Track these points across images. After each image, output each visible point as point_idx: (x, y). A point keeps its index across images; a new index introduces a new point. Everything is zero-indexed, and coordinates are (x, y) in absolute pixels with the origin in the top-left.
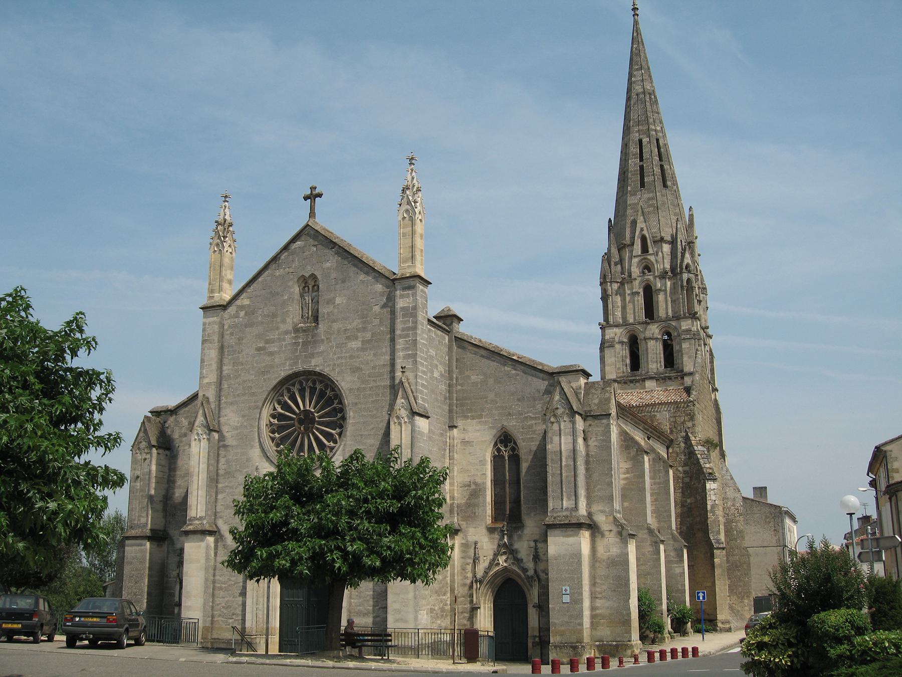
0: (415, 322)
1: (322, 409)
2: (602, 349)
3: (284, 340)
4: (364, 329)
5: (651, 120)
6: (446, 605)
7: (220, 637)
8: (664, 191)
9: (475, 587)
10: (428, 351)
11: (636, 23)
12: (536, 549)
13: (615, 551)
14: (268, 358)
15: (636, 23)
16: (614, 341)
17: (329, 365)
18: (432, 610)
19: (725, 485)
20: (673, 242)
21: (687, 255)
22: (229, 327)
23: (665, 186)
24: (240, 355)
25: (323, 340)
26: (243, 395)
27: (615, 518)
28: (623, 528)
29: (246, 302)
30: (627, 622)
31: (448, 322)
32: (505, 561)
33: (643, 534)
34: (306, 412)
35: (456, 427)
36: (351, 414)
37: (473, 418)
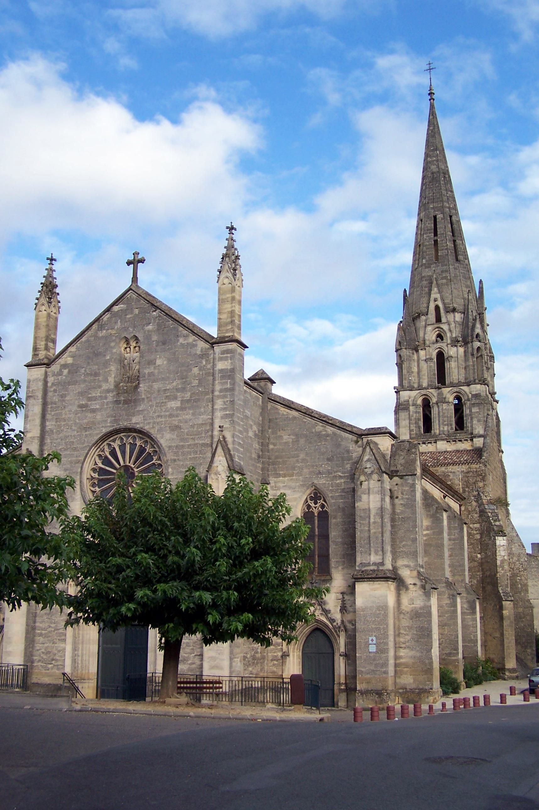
0: (233, 384)
1: (142, 464)
2: (396, 412)
3: (106, 398)
4: (183, 390)
5: (445, 198)
6: (257, 653)
7: (39, 682)
8: (457, 265)
10: (244, 412)
13: (419, 603)
14: (89, 415)
15: (432, 107)
16: (409, 404)
17: (149, 423)
18: (245, 658)
19: (511, 542)
20: (465, 312)
21: (478, 325)
22: (53, 384)
23: (457, 260)
24: (63, 412)
25: (143, 399)
29: (70, 360)
30: (429, 671)
33: (442, 587)
34: (127, 468)
36: (170, 470)
37: (285, 476)
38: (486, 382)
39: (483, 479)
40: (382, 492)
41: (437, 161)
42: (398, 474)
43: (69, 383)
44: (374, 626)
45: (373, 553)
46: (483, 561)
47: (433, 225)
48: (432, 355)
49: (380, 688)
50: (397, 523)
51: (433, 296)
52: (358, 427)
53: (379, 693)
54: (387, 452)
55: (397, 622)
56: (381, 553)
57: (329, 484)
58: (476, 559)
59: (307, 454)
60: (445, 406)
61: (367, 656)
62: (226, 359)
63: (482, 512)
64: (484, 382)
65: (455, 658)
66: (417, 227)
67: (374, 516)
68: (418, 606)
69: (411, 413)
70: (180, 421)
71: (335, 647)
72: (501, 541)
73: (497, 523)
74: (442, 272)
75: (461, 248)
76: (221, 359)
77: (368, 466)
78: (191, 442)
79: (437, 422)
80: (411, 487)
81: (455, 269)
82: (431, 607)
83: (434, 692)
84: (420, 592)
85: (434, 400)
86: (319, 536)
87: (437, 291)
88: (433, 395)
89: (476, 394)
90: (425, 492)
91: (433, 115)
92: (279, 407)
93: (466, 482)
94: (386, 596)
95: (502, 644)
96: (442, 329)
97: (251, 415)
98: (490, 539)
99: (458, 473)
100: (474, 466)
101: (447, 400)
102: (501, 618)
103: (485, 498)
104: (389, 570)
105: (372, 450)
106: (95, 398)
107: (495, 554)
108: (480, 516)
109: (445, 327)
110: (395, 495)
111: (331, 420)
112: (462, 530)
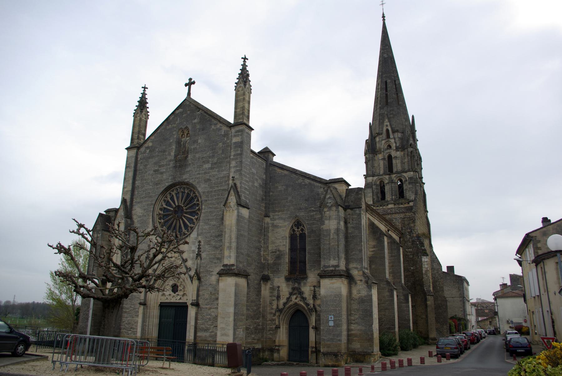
1: (188, 204)
6: (259, 325)
9: (277, 314)
10: (251, 169)
12: (315, 291)
13: (364, 293)
14: (159, 176)
26: (146, 197)
27: (364, 273)
28: (369, 279)
29: (150, 144)
30: (371, 340)
31: (266, 155)
32: (296, 299)
35: (269, 217)
36: (203, 207)
40: (339, 219)
43: (149, 158)
45: (332, 259)
49: (336, 351)
51: (385, 124)
53: (336, 355)
56: (337, 258)
60: (393, 185)
62: (238, 136)
68: (364, 295)
70: (210, 176)
71: (310, 322)
72: (425, 259)
76: (235, 136)
78: (216, 189)
83: (374, 355)
84: (365, 286)
85: (386, 182)
90: (372, 226)
92: (276, 169)
94: (341, 288)
95: (427, 322)
97: (257, 173)
98: (418, 258)
100: (408, 214)
102: (426, 306)
104: (343, 270)
105: (331, 191)
106: (163, 166)
107: (421, 267)
108: (412, 244)
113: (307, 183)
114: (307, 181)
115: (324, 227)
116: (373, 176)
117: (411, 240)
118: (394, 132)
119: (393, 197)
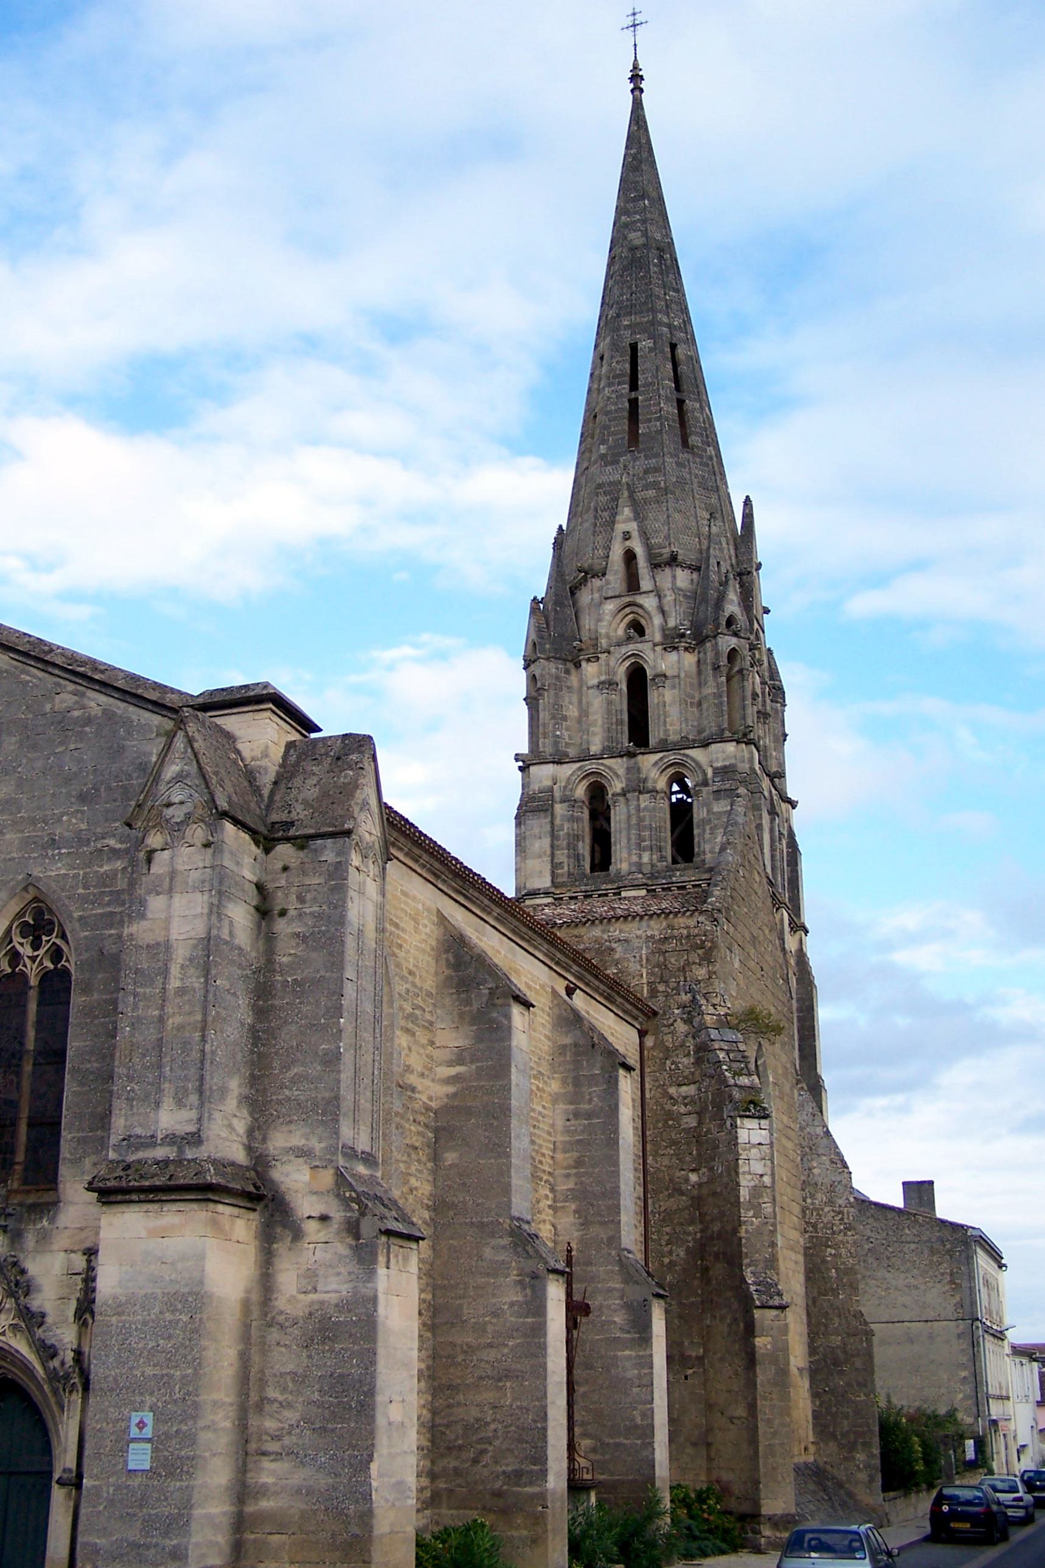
2: (519, 819)
8: (684, 456)
11: (637, 106)
13: (335, 1287)
15: (637, 106)
23: (685, 443)
38: (752, 736)
39: (708, 958)
40: (220, 887)
41: (644, 221)
42: (292, 832)
44: (149, 1371)
45: (168, 1102)
46: (705, 1191)
47: (627, 366)
48: (615, 674)
50: (277, 1002)
51: (620, 528)
52: (183, 690)
54: (264, 762)
55: (256, 1358)
56: (194, 1098)
57: (76, 876)
58: (683, 1187)
59: (19, 785)
60: (645, 801)
61: (118, 1488)
63: (703, 1050)
64: (745, 735)
65: (535, 1489)
66: (592, 375)
67: (182, 967)
68: (333, 1298)
69: (558, 822)
71: (56, 1451)
73: (744, 1081)
74: (646, 472)
75: (697, 420)
77: (176, 799)
79: (624, 841)
80: (331, 877)
81: (679, 464)
82: (374, 1300)
84: (342, 1248)
85: (616, 786)
86: (38, 1053)
87: (631, 515)
88: (616, 774)
89: (725, 767)
91: (637, 123)
93: (658, 966)
94: (201, 1257)
96: (641, 606)
99: (636, 943)
100: (681, 921)
101: (650, 785)
103: (711, 1010)
105: (190, 741)
107: (733, 1169)
108: (698, 1062)
109: (649, 602)
110: (279, 901)
111: (102, 672)
112: (612, 1085)
113: (96, 711)
114: (97, 702)
115: (141, 931)
116: (559, 763)
117: (690, 1044)
118: (656, 565)
119: (646, 858)
